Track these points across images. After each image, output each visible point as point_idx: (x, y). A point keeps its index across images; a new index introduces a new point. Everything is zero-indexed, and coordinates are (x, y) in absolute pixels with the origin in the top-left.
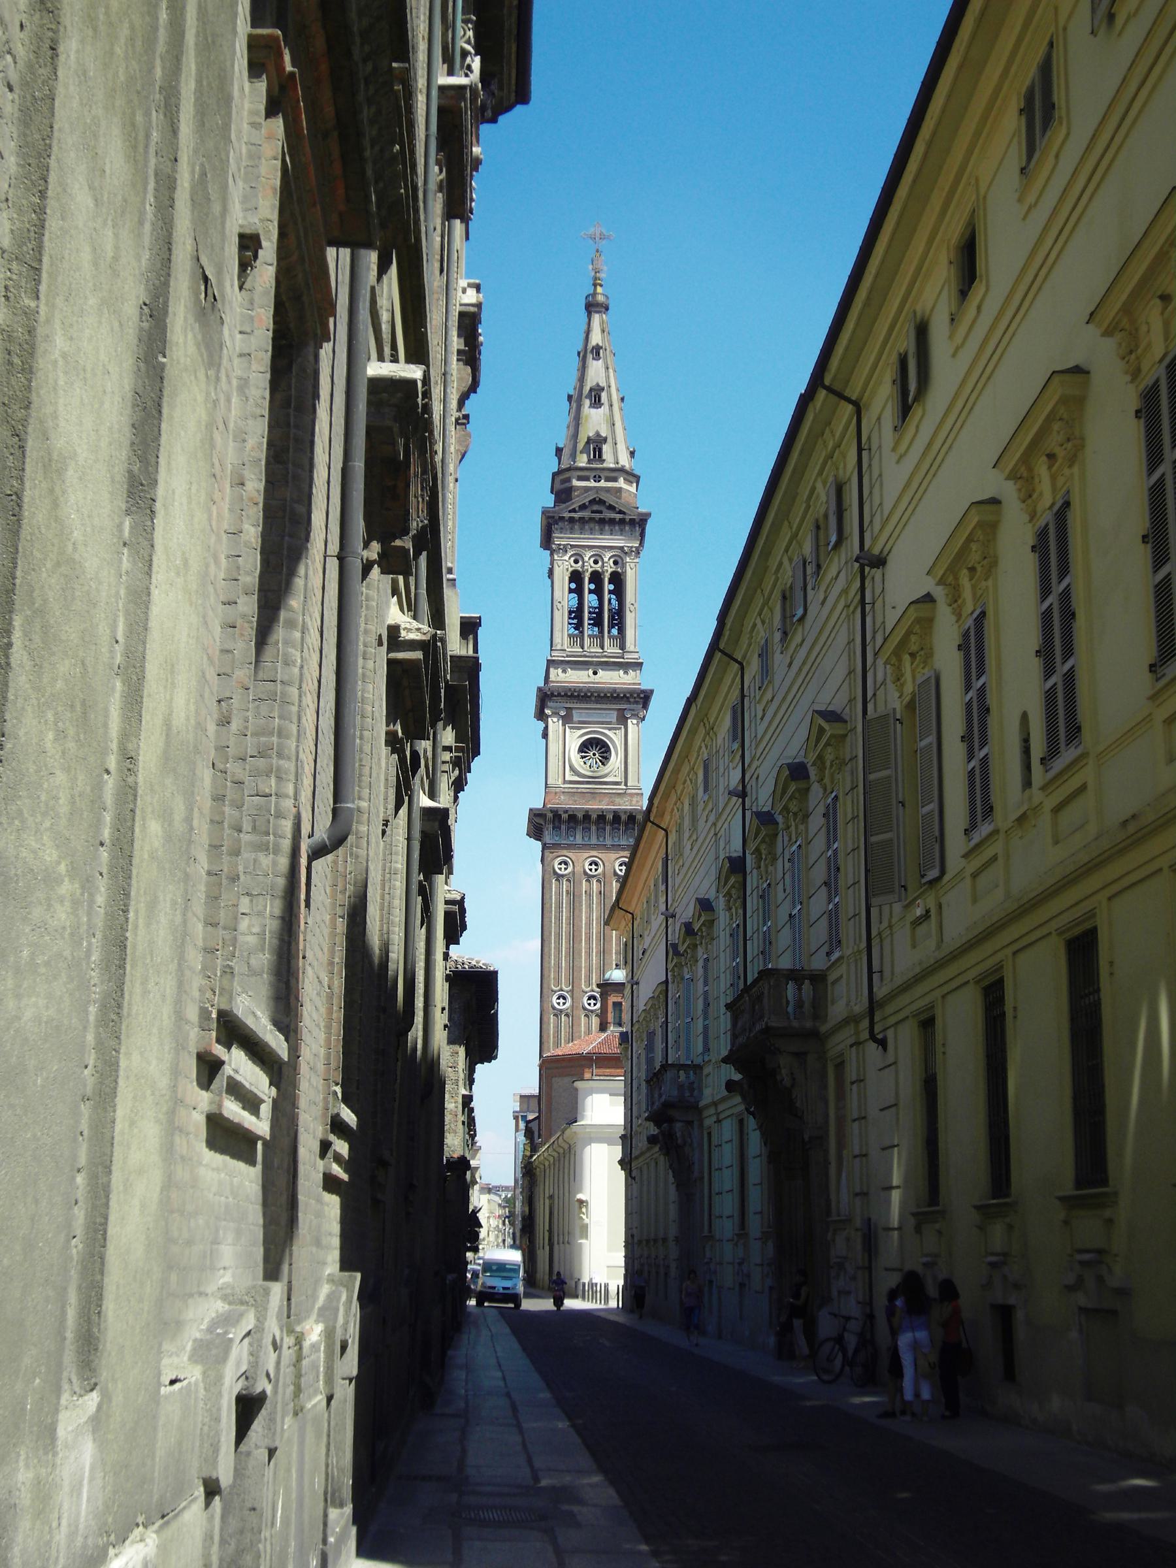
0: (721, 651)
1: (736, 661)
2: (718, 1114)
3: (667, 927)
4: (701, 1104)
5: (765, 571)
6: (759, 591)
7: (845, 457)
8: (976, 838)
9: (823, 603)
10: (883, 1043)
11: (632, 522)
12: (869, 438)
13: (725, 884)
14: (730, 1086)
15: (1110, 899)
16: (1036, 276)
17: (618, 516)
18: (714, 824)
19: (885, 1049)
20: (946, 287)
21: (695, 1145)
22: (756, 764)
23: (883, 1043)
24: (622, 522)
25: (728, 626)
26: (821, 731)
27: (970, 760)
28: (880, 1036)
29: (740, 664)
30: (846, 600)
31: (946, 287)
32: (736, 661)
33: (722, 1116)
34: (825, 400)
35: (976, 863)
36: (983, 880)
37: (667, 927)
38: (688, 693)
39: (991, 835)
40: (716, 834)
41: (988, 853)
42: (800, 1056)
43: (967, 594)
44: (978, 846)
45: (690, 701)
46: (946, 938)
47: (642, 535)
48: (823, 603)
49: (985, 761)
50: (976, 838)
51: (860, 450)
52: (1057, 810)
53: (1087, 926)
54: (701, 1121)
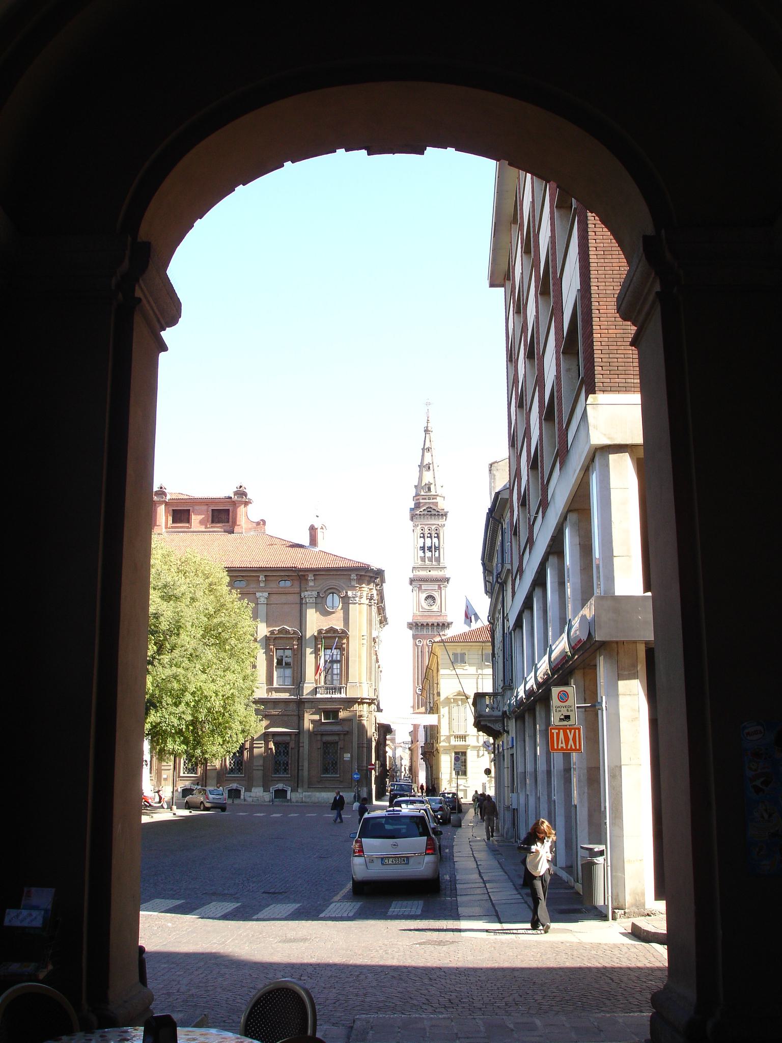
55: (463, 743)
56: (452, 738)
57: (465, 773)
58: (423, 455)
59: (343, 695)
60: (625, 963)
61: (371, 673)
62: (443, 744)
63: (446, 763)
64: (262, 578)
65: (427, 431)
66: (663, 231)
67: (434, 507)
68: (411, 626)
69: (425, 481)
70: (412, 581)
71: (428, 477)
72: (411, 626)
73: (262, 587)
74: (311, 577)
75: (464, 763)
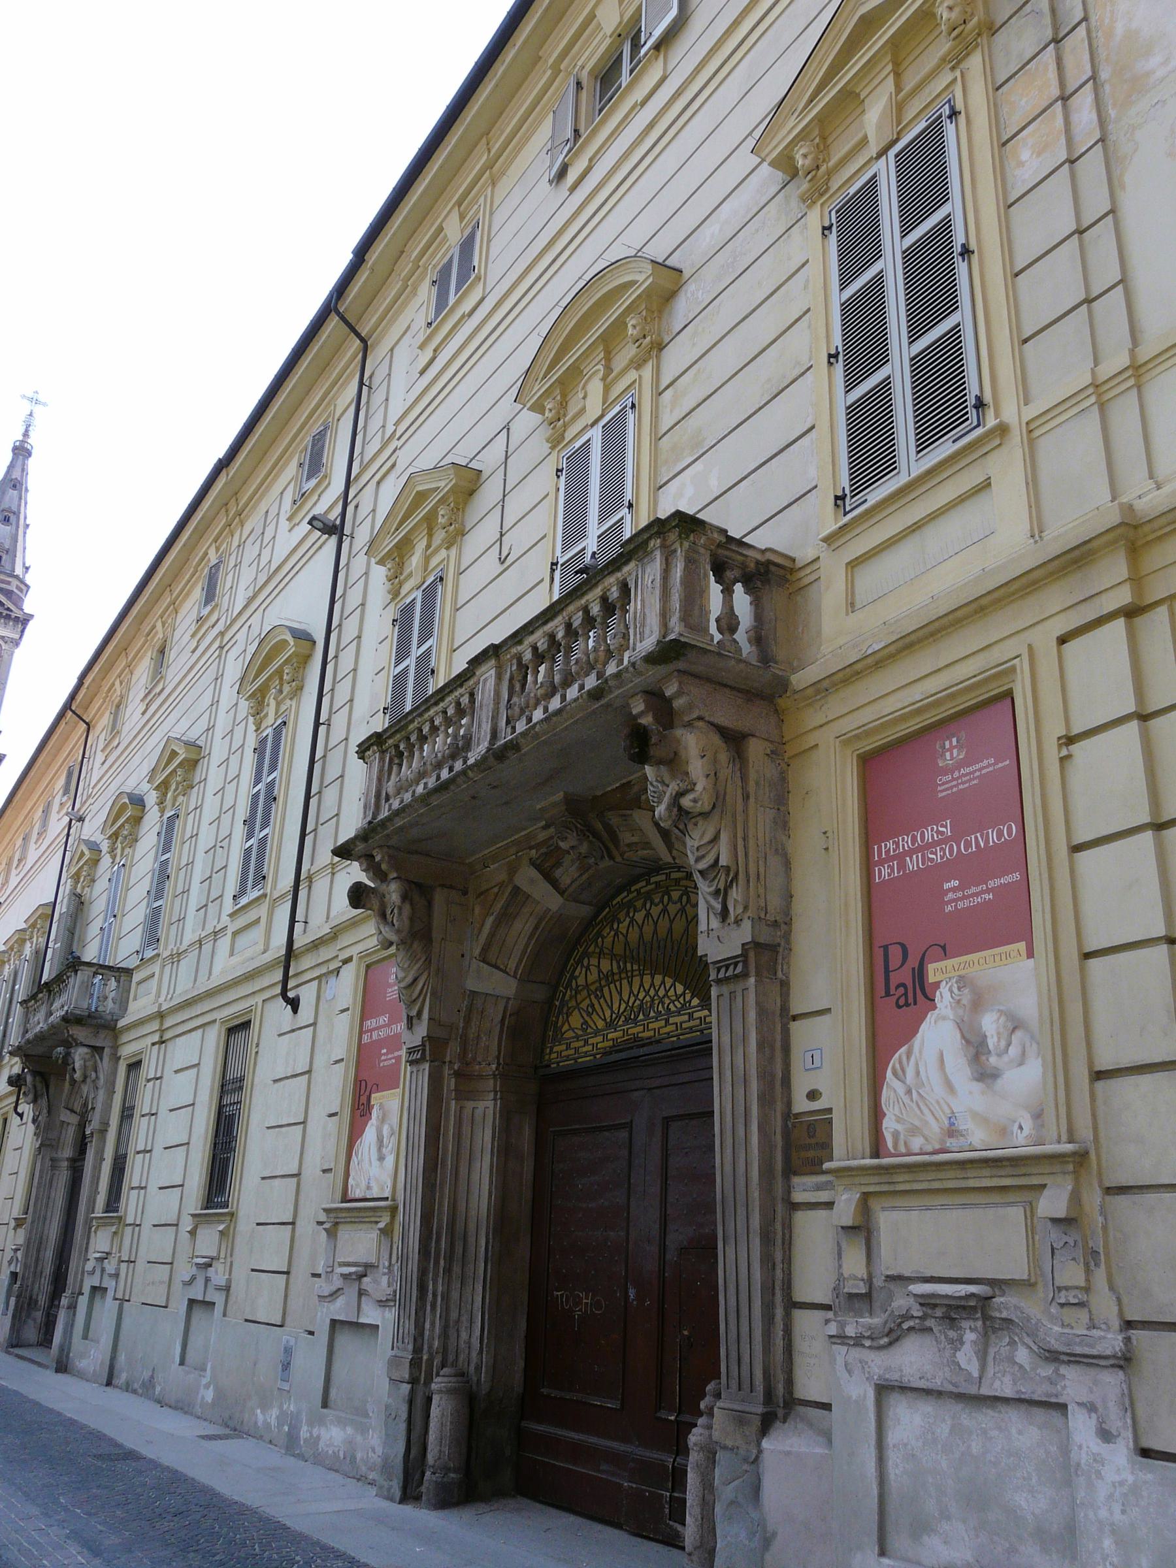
0: (338, 313)
1: (358, 335)
2: (162, 1031)
3: (68, 835)
4: (121, 1023)
5: (535, 64)
6: (484, 140)
7: (494, 184)
8: (244, 901)
9: (193, 652)
10: (294, 1004)
11: (17, 619)
12: (371, 377)
13: (113, 824)
14: (358, 896)
15: (1062, 640)
16: (606, 201)
17: (5, 612)
18: (222, 634)
19: (295, 1010)
20: (293, 483)
21: (102, 1081)
22: (91, 801)
23: (294, 1004)
24: (8, 617)
25: (86, 685)
26: (83, 854)
27: (249, 837)
28: (291, 995)
29: (87, 724)
30: (221, 642)
31: (293, 483)
32: (358, 335)
33: (167, 1035)
34: (335, 327)
35: (241, 922)
36: (242, 941)
37: (68, 835)
38: (221, 451)
39: (258, 899)
40: (221, 647)
41: (251, 916)
42: (734, 740)
43: (271, 710)
44: (243, 907)
45: (222, 465)
46: (332, 915)
47: (23, 631)
48: (193, 652)
49: (263, 842)
50: (244, 901)
51: (361, 383)
52: (235, 934)
53: (246, 1019)
54: (115, 1048)
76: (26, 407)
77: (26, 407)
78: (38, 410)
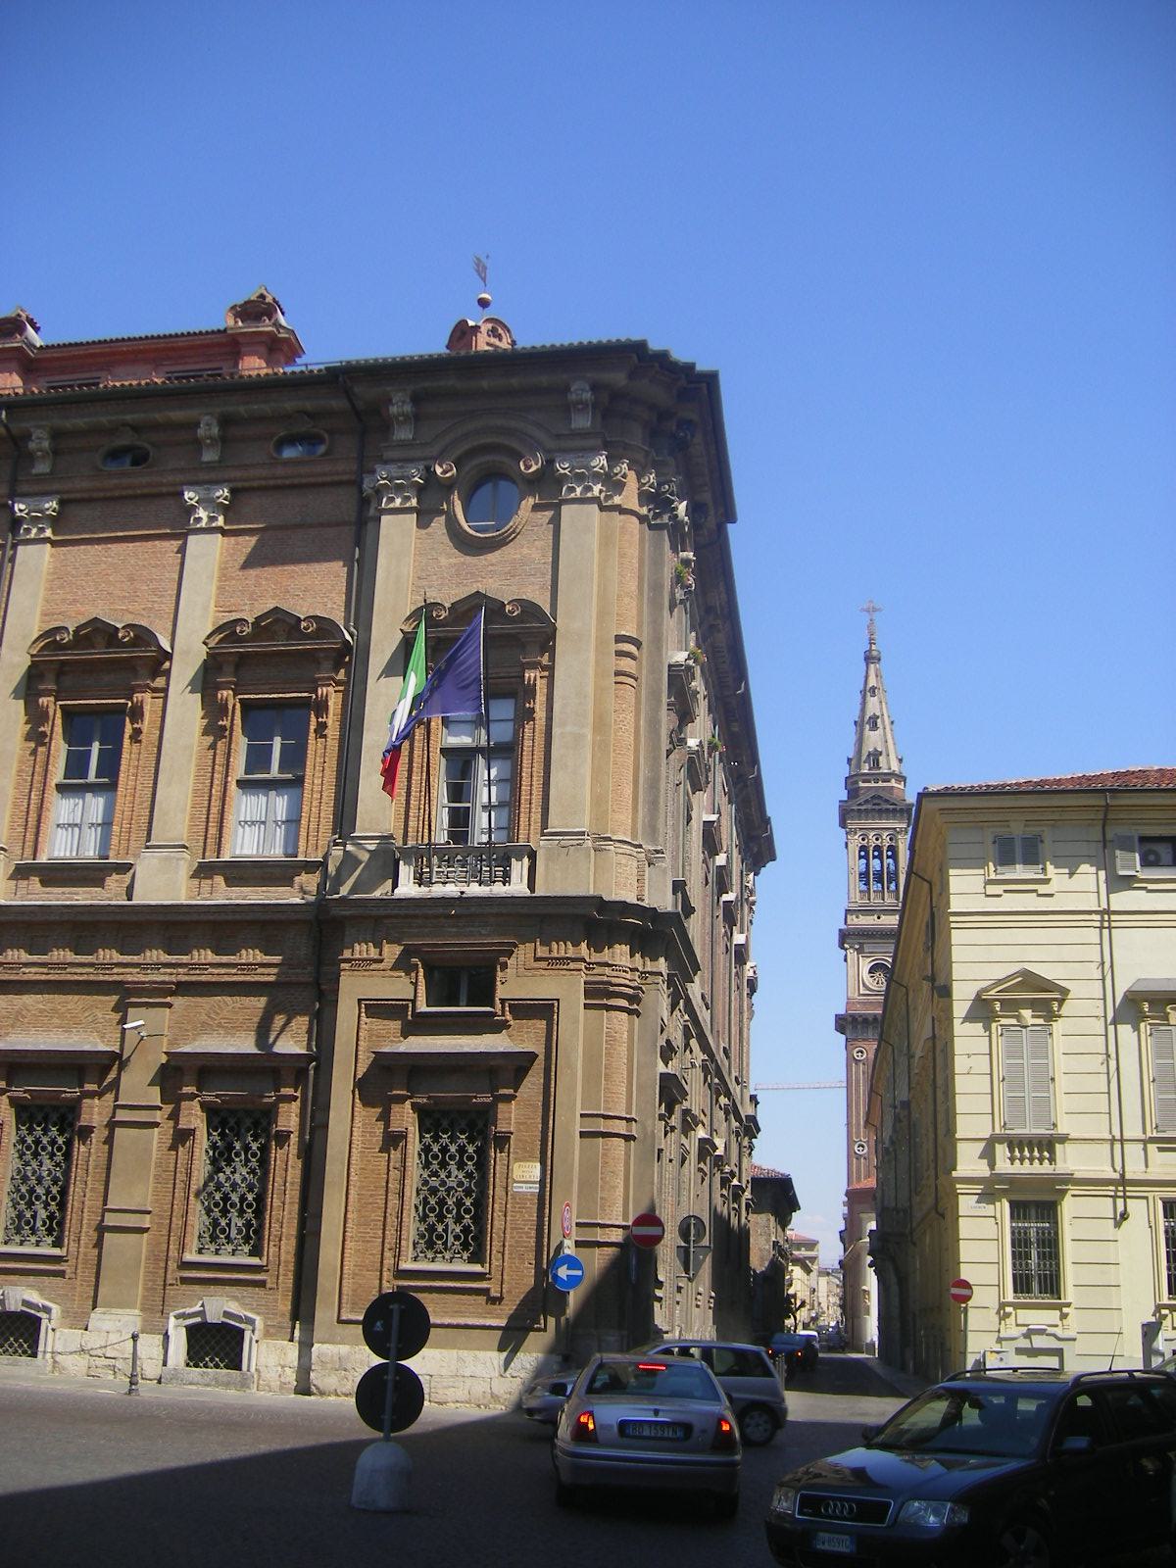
55: (1046, 1168)
56: (1001, 1151)
57: (1051, 1284)
58: (864, 703)
59: (518, 887)
60: (828, 1396)
61: (653, 805)
62: (969, 1163)
63: (982, 1243)
64: (208, 428)
65: (869, 659)
66: (1020, 979)
67: (886, 796)
68: (843, 1024)
69: (868, 748)
70: (845, 937)
71: (873, 739)
72: (843, 1024)
73: (210, 467)
74: (400, 405)
75: (1050, 1246)
76: (865, 618)
77: (865, 618)
78: (876, 616)
